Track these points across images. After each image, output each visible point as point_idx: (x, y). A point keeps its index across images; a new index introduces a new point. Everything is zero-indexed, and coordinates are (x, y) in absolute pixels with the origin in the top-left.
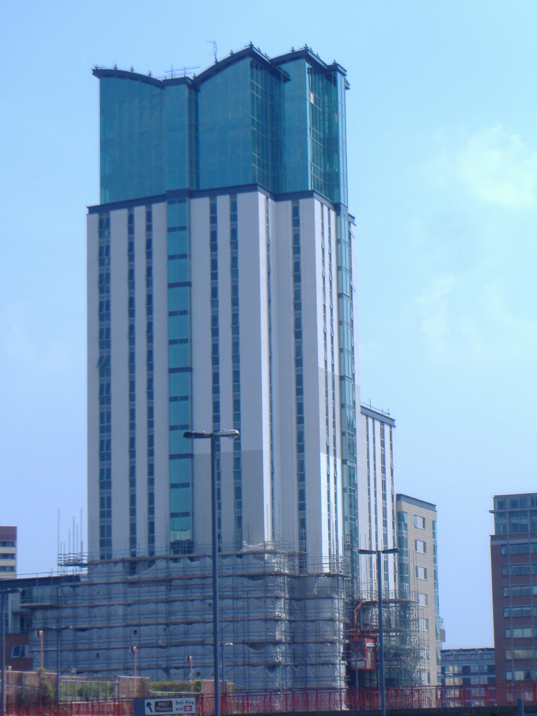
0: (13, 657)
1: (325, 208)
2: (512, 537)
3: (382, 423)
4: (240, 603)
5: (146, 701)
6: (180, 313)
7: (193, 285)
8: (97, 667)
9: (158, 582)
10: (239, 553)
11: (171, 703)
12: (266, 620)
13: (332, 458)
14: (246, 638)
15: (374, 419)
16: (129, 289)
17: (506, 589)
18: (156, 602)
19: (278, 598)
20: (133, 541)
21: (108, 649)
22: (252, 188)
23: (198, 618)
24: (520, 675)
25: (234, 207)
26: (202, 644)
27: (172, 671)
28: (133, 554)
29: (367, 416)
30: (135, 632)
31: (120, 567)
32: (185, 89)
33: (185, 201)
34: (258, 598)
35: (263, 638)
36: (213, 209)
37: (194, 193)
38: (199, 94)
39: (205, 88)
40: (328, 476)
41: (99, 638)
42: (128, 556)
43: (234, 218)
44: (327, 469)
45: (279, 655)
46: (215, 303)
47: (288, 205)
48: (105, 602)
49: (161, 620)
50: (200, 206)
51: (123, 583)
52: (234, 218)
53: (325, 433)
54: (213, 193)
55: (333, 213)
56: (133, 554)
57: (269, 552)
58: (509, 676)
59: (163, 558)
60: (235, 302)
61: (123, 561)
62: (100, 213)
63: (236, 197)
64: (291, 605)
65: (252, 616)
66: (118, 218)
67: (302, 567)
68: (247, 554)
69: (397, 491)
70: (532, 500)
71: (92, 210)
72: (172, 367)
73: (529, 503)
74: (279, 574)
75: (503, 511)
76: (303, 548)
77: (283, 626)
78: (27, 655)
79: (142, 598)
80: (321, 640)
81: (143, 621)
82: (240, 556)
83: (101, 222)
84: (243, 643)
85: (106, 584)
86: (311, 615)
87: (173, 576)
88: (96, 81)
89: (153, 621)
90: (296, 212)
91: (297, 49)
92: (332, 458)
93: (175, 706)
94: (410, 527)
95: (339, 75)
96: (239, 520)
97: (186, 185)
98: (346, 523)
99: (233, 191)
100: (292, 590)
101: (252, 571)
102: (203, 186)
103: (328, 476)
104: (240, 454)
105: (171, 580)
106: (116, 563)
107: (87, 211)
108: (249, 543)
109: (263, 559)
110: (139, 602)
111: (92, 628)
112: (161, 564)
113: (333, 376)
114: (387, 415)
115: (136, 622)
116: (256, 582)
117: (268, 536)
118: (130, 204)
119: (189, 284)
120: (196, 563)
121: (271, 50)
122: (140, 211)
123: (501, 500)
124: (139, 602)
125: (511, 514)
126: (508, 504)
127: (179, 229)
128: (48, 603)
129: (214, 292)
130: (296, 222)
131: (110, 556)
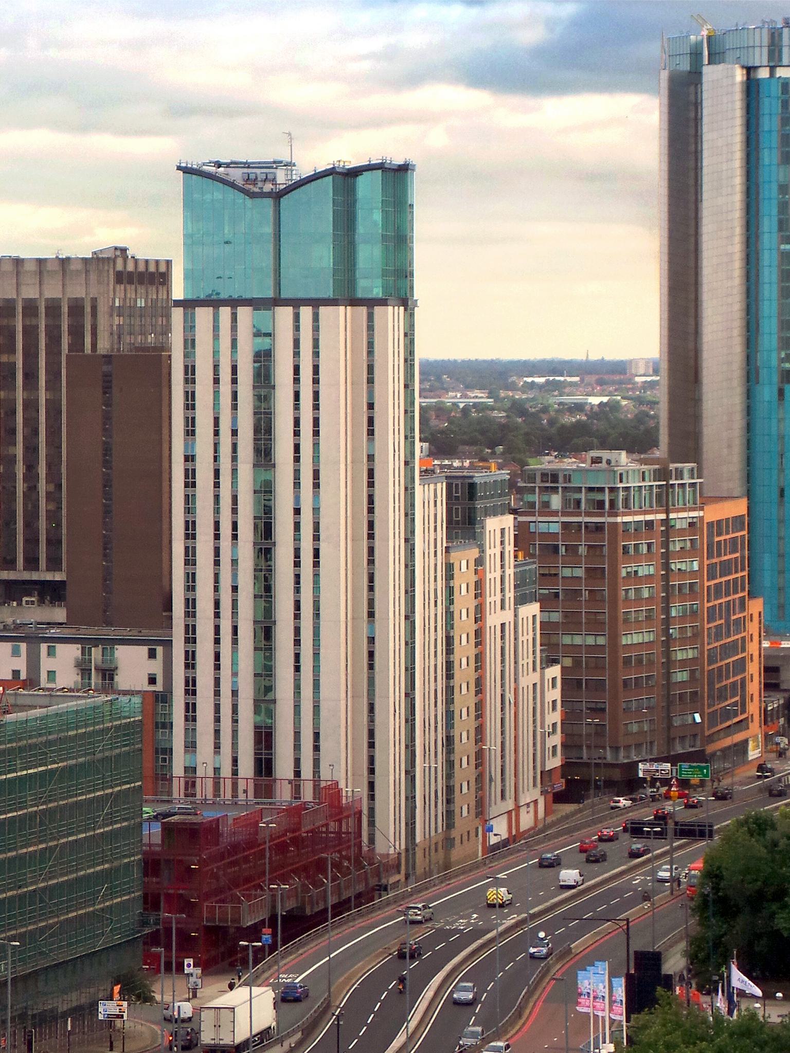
37: (277, 302)
39: (284, 201)
43: (316, 329)
47: (363, 310)
50: (284, 314)
52: (316, 329)
54: (296, 303)
90: (370, 317)
99: (316, 303)
122: (225, 312)
130: (370, 328)
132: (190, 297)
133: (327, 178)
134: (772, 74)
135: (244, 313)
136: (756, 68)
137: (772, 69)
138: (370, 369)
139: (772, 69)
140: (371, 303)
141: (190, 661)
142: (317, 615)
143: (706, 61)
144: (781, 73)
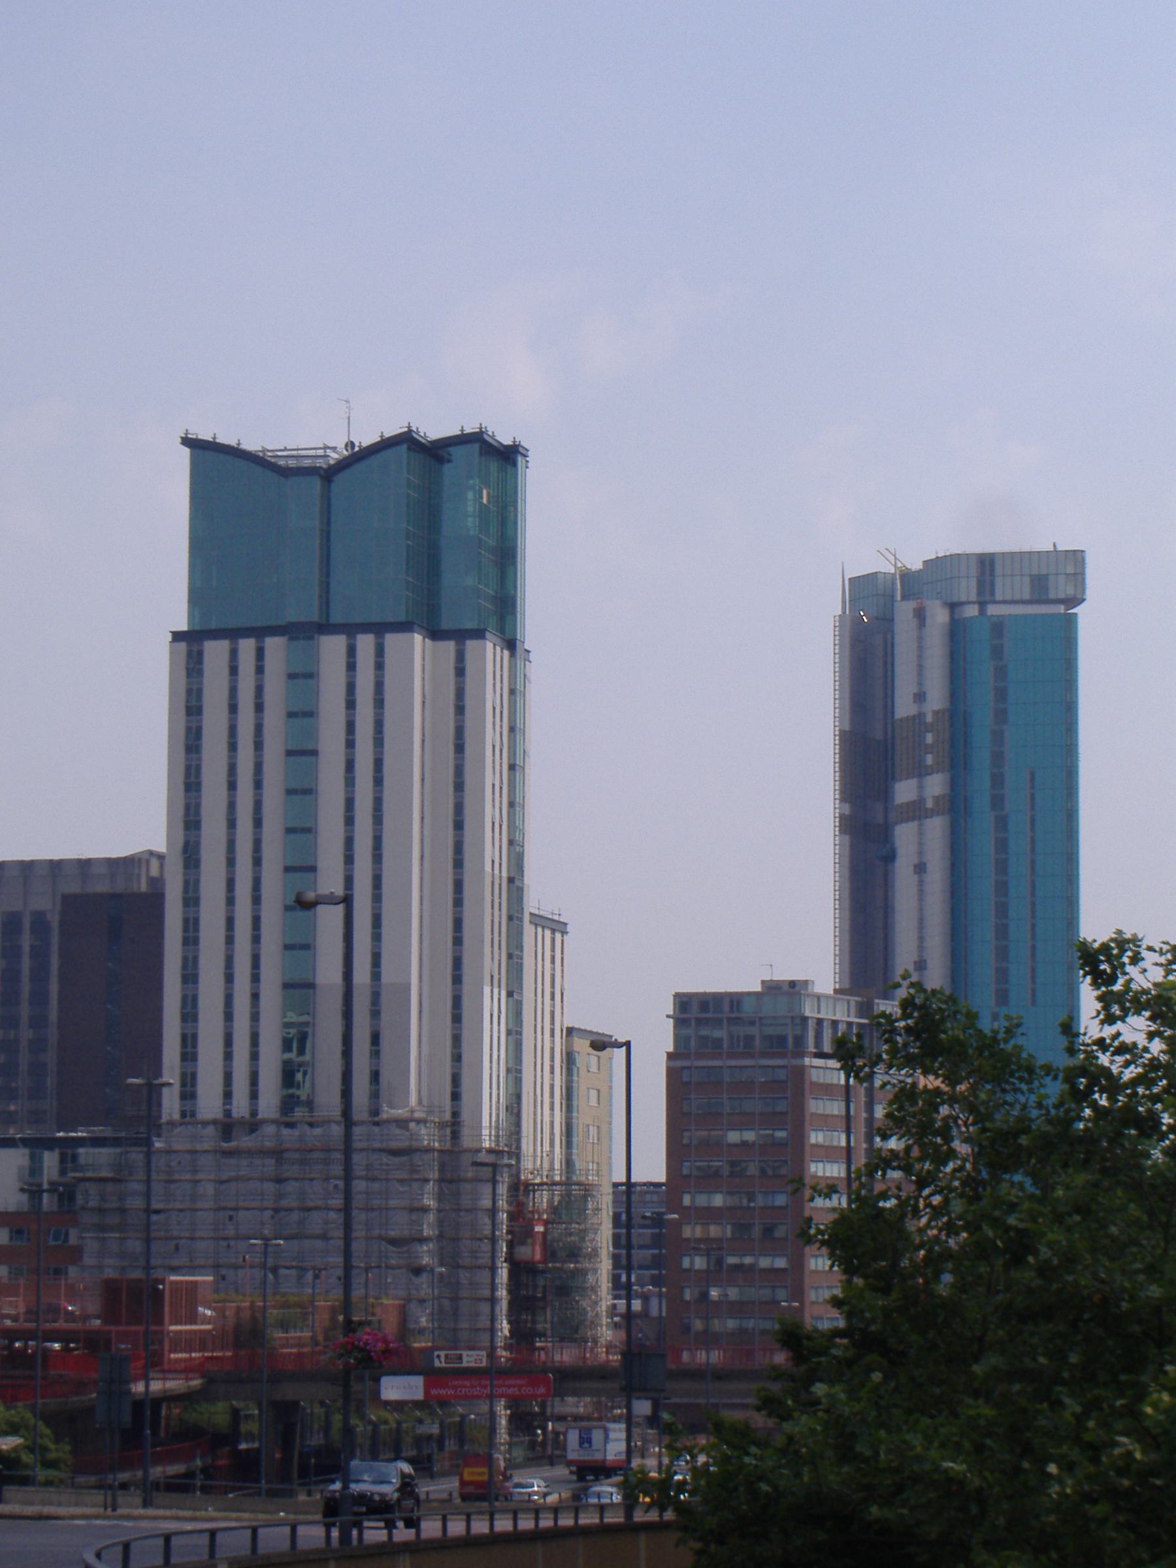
0: (52, 1243)
1: (498, 649)
2: (699, 1056)
3: (553, 931)
4: (376, 1186)
5: (436, 1353)
6: (302, 792)
7: (321, 756)
8: (175, 1263)
9: (263, 1153)
10: (376, 1119)
11: (461, 1356)
12: (412, 1210)
13: (496, 991)
14: (383, 1232)
15: (543, 927)
16: (229, 751)
17: (686, 1134)
18: (262, 1180)
19: (427, 1181)
20: (228, 1095)
21: (192, 1239)
22: (405, 627)
23: (319, 1203)
24: (700, 1263)
25: (380, 652)
26: (324, 1237)
27: (282, 1271)
28: (228, 1113)
29: (536, 925)
30: (231, 1218)
31: (210, 1130)
32: (317, 483)
33: (311, 638)
34: (401, 1181)
35: (406, 1233)
36: (351, 651)
37: (325, 628)
38: (333, 485)
39: (339, 479)
40: (492, 1015)
41: (179, 1223)
42: (219, 1115)
43: (379, 666)
44: (491, 1004)
45: (426, 1255)
46: (350, 781)
47: (450, 646)
48: (188, 1176)
49: (266, 1204)
50: (333, 647)
51: (215, 1152)
52: (379, 666)
53: (488, 958)
54: (351, 630)
55: (506, 653)
56: (228, 1113)
57: (418, 1121)
58: (686, 1263)
59: (274, 1121)
60: (378, 781)
61: (214, 1122)
62: (190, 642)
63: (383, 638)
64: (440, 1188)
65: (393, 1203)
66: (216, 652)
67: (455, 1135)
68: (388, 1121)
69: (568, 1023)
70: (732, 1002)
71: (177, 636)
72: (289, 864)
73: (726, 1008)
74: (428, 1150)
75: (686, 1016)
76: (455, 1114)
77: (431, 1217)
78: (73, 1240)
79: (242, 1173)
80: (478, 1236)
81: (241, 1204)
82: (377, 1124)
83: (190, 654)
84: (381, 1238)
85: (189, 1152)
86: (466, 1202)
87: (285, 1146)
88: (187, 451)
89: (257, 1204)
90: (460, 657)
91: (468, 430)
92: (496, 991)
93: (465, 1359)
94: (583, 1072)
95: (520, 458)
96: (375, 1076)
97: (315, 618)
98: (510, 1076)
99: (380, 629)
100: (442, 1167)
101: (394, 1145)
102: (337, 618)
103: (492, 1015)
104: (379, 986)
105: (282, 1152)
106: (205, 1124)
107: (169, 637)
108: (391, 1106)
109: (407, 1129)
110: (237, 1179)
111: (169, 1210)
112: (270, 1129)
113: (501, 878)
114: (556, 918)
115: (232, 1204)
116: (397, 1160)
117: (413, 1100)
118: (233, 634)
119: (314, 753)
120: (318, 1131)
121: (433, 429)
122: (247, 646)
123: (684, 999)
124: (237, 1179)
125: (699, 1021)
126: (695, 1007)
127: (303, 676)
128: (104, 1174)
129: (350, 766)
130: (460, 672)
131: (193, 1114)
132: (197, 628)
133: (398, 448)
134: (982, 611)
135: (275, 645)
136: (962, 604)
137: (982, 605)
138: (458, 924)
139: (982, 605)
140: (461, 636)
141: (189, 1049)
142: (379, 741)
143: (899, 598)
144: (992, 610)
